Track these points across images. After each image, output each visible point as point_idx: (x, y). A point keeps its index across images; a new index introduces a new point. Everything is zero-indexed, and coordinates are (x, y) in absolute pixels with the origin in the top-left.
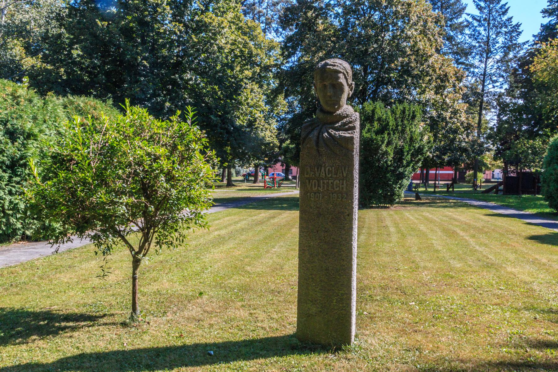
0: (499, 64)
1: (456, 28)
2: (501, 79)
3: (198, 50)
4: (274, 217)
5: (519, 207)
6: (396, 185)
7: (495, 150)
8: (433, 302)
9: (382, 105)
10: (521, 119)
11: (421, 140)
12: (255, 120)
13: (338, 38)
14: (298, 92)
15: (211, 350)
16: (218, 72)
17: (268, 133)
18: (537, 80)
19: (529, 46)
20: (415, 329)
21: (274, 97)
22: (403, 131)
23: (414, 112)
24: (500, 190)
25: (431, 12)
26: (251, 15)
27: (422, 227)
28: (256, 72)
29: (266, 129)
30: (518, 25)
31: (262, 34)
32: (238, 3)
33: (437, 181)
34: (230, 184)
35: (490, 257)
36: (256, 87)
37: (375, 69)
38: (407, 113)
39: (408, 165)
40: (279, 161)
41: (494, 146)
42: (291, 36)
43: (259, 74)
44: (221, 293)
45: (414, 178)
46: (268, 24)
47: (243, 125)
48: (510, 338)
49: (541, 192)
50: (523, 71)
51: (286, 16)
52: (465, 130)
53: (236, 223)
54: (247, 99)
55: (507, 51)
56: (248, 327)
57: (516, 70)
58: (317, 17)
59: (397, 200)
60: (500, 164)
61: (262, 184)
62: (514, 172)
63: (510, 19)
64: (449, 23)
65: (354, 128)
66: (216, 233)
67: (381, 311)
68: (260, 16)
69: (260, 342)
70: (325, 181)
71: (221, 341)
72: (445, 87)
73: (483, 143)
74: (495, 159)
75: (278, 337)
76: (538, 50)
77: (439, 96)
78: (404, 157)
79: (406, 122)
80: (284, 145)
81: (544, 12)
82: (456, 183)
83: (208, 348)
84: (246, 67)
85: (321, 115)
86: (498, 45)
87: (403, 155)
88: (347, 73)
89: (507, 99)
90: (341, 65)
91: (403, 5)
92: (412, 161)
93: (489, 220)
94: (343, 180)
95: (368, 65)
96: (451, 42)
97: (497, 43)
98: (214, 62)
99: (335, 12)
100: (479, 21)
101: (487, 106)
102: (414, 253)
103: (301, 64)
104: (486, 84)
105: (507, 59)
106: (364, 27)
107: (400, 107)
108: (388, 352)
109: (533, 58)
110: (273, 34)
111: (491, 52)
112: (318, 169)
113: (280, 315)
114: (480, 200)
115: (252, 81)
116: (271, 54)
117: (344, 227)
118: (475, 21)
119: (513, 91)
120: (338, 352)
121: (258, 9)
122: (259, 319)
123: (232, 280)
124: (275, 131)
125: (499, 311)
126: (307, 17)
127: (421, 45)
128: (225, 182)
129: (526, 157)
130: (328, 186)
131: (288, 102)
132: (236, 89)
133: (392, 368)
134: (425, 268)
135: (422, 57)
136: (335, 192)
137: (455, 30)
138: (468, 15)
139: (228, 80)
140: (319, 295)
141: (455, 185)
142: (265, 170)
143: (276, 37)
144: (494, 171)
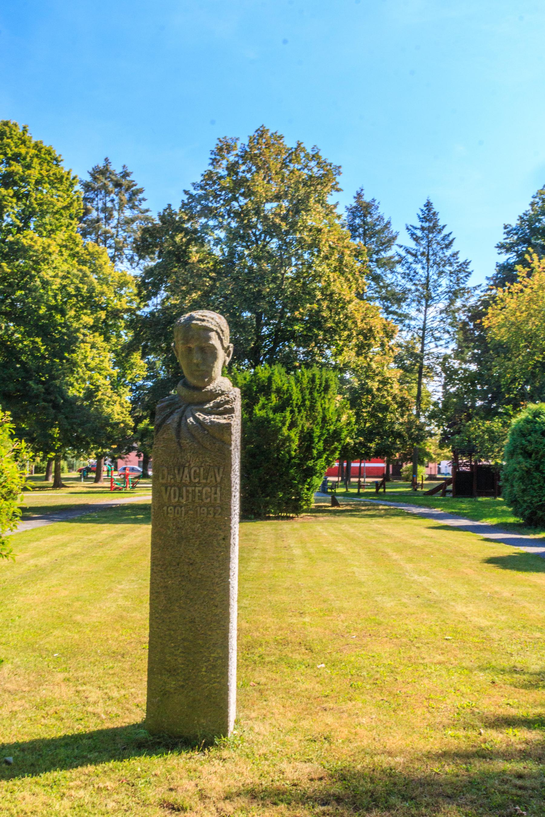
0: (443, 315)
1: (385, 264)
2: (446, 336)
3: (11, 285)
4: (123, 535)
5: (474, 516)
6: (303, 485)
7: (441, 434)
8: (350, 662)
9: (283, 370)
10: (475, 391)
11: (338, 420)
12: (97, 388)
13: (219, 273)
14: (161, 349)
15: (10, 755)
16: (40, 317)
17: (117, 408)
18: (492, 339)
19: (482, 292)
20: (325, 705)
21: (127, 356)
22: (312, 408)
23: (327, 381)
24: (449, 491)
25: (349, 241)
26: (93, 236)
27: (340, 548)
28: (100, 318)
29: (115, 402)
30: (466, 263)
31: (110, 263)
32: (73, 219)
33: (362, 477)
34: (58, 484)
35: (433, 590)
36: (99, 339)
37: (272, 318)
38: (317, 381)
39: (320, 456)
40: (133, 449)
41: (439, 428)
42: (151, 269)
43: (104, 322)
44: (32, 659)
45: (329, 474)
46: (119, 249)
47: (79, 397)
48: (458, 714)
49: (502, 495)
50: (474, 325)
51: (143, 239)
52: (399, 407)
53: (65, 545)
54: (86, 357)
55: (454, 298)
56: (73, 713)
57: (465, 324)
58: (188, 243)
59: (305, 507)
60: (448, 454)
61: (108, 484)
62: (467, 466)
63: (455, 255)
64: (375, 257)
65: (232, 411)
66: (32, 562)
67: (275, 680)
68: (106, 238)
69: (89, 738)
70: (190, 489)
71: (27, 739)
72: (370, 346)
73: (424, 424)
74: (441, 445)
75: (117, 728)
76: (493, 298)
77: (361, 358)
78: (313, 445)
79: (316, 394)
80: (141, 426)
81: (501, 246)
82: (388, 480)
83: (4, 752)
84: (85, 311)
85: (184, 392)
86: (440, 289)
87: (313, 442)
88: (222, 331)
89: (454, 363)
90: (214, 320)
91: (310, 230)
92: (325, 450)
93: (434, 535)
94: (216, 487)
95: (261, 313)
96: (378, 283)
97: (440, 286)
98: (35, 304)
99: (216, 237)
100: (415, 255)
101: (428, 372)
102: (326, 588)
103: (167, 308)
104: (426, 342)
105: (453, 308)
106: (257, 259)
107: (308, 374)
108: (283, 744)
109: (486, 308)
110: (126, 264)
111: (432, 299)
112: (179, 470)
113: (123, 692)
114: (420, 506)
115: (94, 332)
116: (122, 292)
117: (218, 556)
118: (409, 256)
119: (462, 352)
120: (208, 749)
121: (104, 227)
122: (89, 699)
123: (52, 638)
124: (128, 405)
125: (444, 673)
126: (175, 242)
127: (335, 287)
128: (51, 481)
129: (482, 443)
130: (194, 496)
131: (148, 363)
132: (69, 343)
133: (287, 770)
134: (341, 610)
135: (337, 303)
136: (204, 506)
137: (382, 267)
138: (401, 247)
139: (57, 329)
140: (180, 660)
141: (387, 483)
142: (112, 462)
143: (131, 270)
144: (440, 464)
